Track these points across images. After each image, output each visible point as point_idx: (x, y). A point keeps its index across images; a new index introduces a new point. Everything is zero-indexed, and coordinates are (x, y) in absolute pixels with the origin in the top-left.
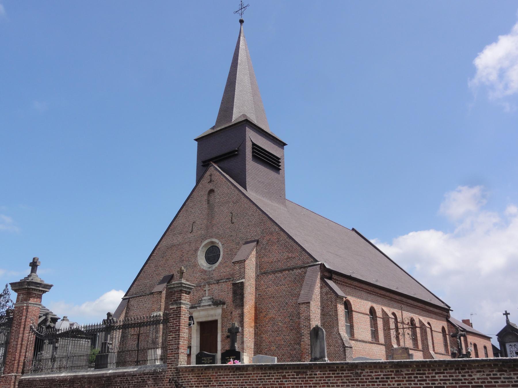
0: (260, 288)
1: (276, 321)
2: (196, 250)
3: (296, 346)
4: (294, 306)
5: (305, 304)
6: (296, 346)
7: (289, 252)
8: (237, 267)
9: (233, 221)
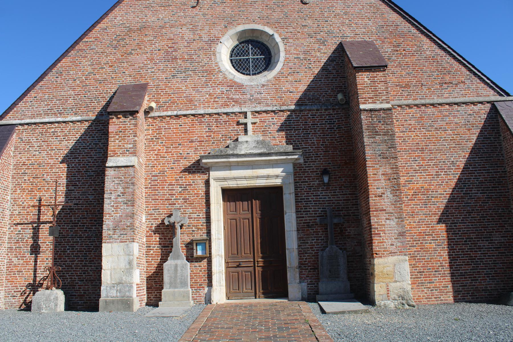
1: (432, 194)
2: (215, 41)
3: (481, 244)
4: (471, 169)
6: (481, 244)
8: (366, 80)
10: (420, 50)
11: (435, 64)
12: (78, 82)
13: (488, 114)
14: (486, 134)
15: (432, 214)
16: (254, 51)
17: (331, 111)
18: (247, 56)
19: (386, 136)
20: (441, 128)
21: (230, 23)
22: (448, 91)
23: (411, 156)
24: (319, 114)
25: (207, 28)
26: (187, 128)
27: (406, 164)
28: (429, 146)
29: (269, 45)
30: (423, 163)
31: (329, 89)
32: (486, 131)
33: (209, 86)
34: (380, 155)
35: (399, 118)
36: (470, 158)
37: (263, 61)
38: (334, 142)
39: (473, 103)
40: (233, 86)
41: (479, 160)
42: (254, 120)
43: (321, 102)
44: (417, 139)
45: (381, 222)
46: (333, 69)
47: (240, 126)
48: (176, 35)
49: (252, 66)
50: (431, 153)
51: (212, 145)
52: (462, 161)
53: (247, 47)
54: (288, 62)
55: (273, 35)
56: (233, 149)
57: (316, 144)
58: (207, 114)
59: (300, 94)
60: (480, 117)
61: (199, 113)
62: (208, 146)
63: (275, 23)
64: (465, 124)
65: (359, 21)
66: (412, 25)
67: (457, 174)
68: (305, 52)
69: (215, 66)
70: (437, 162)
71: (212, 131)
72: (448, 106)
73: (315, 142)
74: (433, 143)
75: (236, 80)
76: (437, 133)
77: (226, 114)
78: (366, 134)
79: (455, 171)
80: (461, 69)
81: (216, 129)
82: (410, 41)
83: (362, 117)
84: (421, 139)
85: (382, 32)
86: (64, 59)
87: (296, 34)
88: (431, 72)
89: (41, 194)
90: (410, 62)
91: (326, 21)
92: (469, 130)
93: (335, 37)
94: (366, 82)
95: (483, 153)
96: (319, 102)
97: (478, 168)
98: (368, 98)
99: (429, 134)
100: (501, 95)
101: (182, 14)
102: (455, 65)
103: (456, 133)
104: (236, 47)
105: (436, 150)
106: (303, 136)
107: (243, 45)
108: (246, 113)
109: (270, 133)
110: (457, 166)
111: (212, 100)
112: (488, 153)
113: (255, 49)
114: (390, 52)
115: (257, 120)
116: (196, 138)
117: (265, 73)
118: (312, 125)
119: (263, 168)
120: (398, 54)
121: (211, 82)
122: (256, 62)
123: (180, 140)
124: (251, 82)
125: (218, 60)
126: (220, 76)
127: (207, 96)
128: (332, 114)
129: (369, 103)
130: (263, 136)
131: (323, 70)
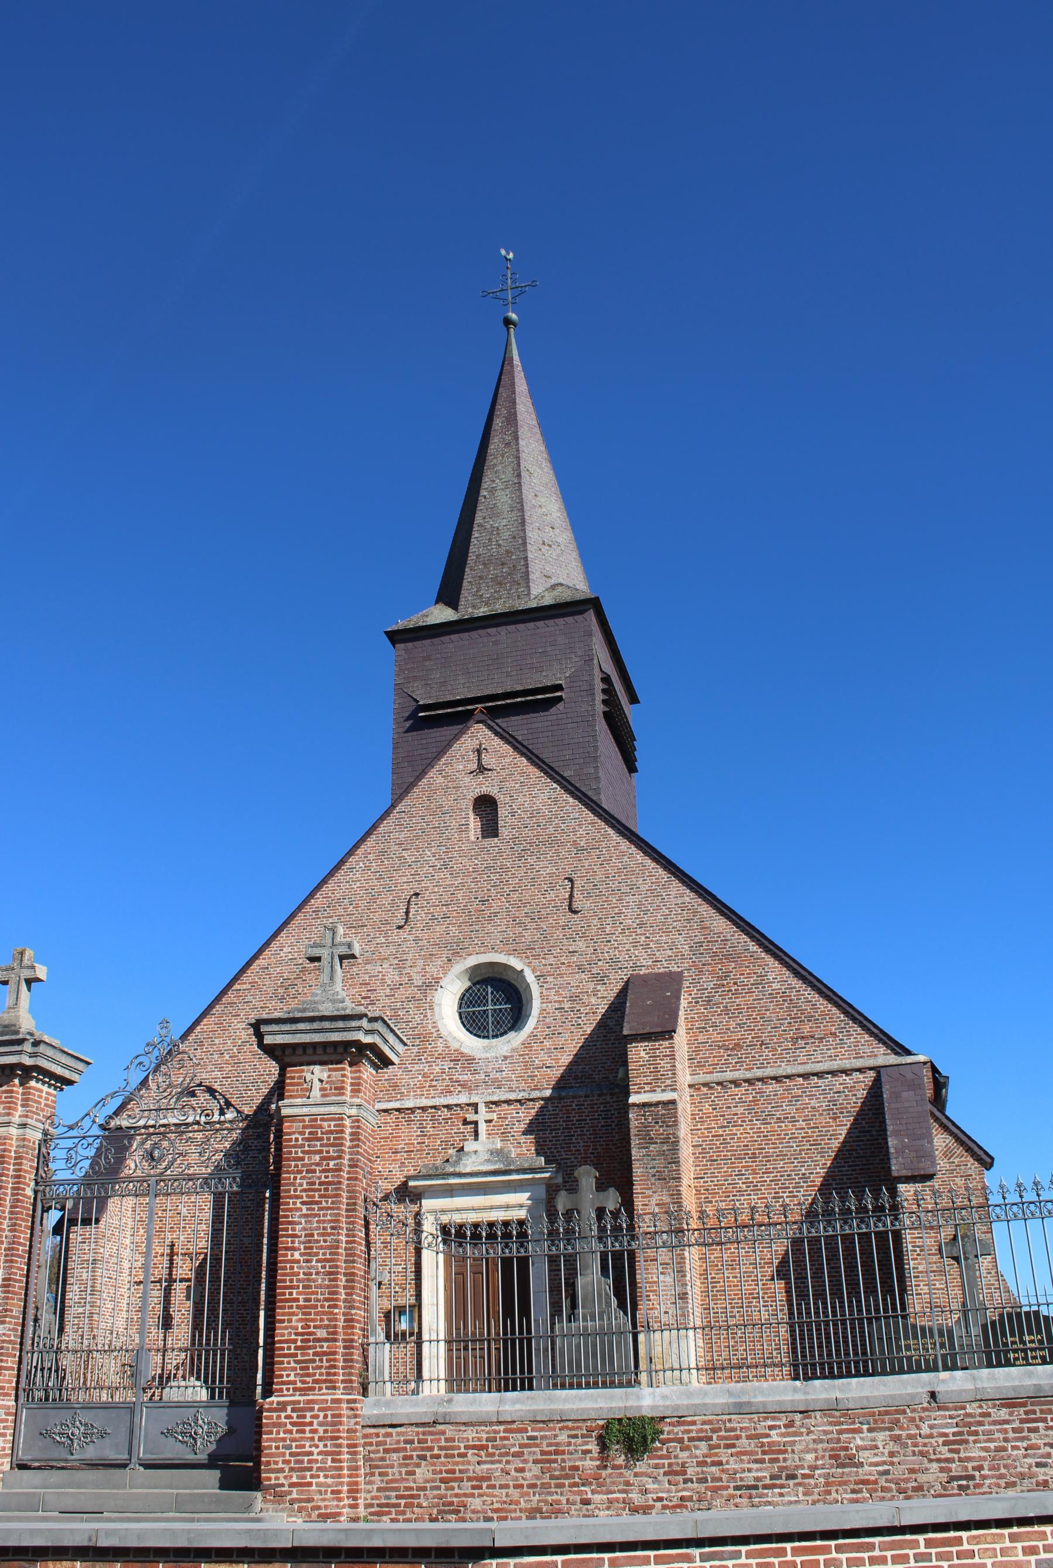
0: (699, 1127)
2: (432, 985)
5: (919, 1179)
7: (804, 1021)
8: (643, 1054)
9: (575, 906)
10: (761, 981)
11: (786, 1005)
12: (227, 1057)
13: (870, 1089)
14: (864, 1125)
15: (765, 1263)
16: (495, 996)
17: (608, 1098)
18: (484, 1005)
19: (665, 1145)
20: (788, 1118)
21: (456, 952)
22: (807, 1051)
23: (735, 1167)
24: (589, 1102)
25: (420, 963)
26: (388, 1130)
27: (725, 1180)
28: (765, 1149)
29: (519, 987)
30: (753, 1178)
31: (609, 1059)
32: (864, 1119)
33: (423, 1061)
34: (654, 1176)
35: (718, 1104)
36: (834, 1167)
37: (509, 1014)
38: (611, 1149)
39: (846, 1072)
40: (459, 1060)
41: (849, 1171)
42: (489, 1116)
43: (594, 1082)
44: (747, 1138)
45: (652, 1278)
46: (615, 1025)
47: (469, 1127)
48: (374, 976)
49: (493, 1023)
50: (769, 1161)
51: (426, 1158)
52: (820, 1173)
53: (484, 990)
54: (545, 1017)
55: (522, 970)
56: (454, 1166)
57: (582, 1151)
58: (419, 1108)
59: (561, 1070)
60: (855, 1095)
61: (406, 1106)
62: (420, 1158)
63: (527, 949)
64: (828, 1110)
65: (662, 936)
66: (750, 938)
67: (810, 1195)
68: (572, 997)
69: (433, 1027)
70: (777, 1176)
71: (426, 1135)
72: (801, 1079)
73: (582, 1148)
74: (773, 1144)
75: (463, 1050)
76: (779, 1127)
77: (448, 1107)
78: (634, 1142)
79: (807, 1191)
80: (831, 1010)
81: (432, 1131)
82: (746, 967)
83: (630, 1116)
84: (753, 1137)
85: (700, 954)
86: (205, 1020)
87: (559, 968)
88: (779, 1020)
89: (174, 1236)
90: (744, 1005)
91: (608, 941)
92: (834, 1119)
93: (621, 968)
94: (643, 1057)
95: (858, 1157)
96: (592, 1082)
97: (846, 1183)
98: (645, 1084)
99: (767, 1128)
100: (897, 1053)
101: (383, 940)
102: (821, 1004)
103: (812, 1125)
104: (467, 991)
105: (777, 1156)
106: (563, 1140)
107: (478, 987)
108: (477, 1104)
109: (513, 1136)
110: (811, 1182)
111: (428, 1084)
112: (865, 1157)
113: (497, 993)
114: (712, 988)
115: (494, 1116)
116: (403, 1146)
117: (512, 1035)
118: (577, 1120)
119: (501, 1194)
120: (724, 991)
121: (425, 1054)
122: (498, 1015)
123: (378, 1150)
124: (487, 1052)
125: (437, 1017)
126: (440, 1044)
127: (420, 1078)
128: (609, 1103)
129: (645, 1092)
130: (501, 1141)
131: (599, 1027)
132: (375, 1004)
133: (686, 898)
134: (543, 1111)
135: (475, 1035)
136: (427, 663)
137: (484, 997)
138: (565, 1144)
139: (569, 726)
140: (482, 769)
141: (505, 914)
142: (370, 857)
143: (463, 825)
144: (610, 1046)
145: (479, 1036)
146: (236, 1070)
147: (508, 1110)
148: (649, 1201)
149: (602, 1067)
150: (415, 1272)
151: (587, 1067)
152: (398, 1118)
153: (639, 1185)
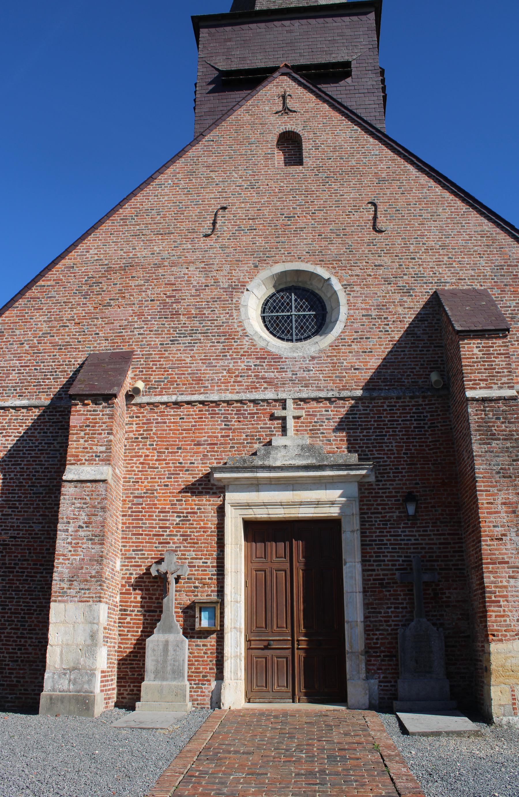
8: (476, 351)
9: (379, 226)
12: (27, 347)
16: (299, 304)
17: (420, 400)
18: (288, 311)
19: (508, 442)
25: (227, 267)
26: (191, 422)
29: (322, 296)
31: (417, 365)
33: (228, 357)
34: (498, 473)
37: (312, 320)
38: (424, 450)
40: (265, 358)
42: (298, 413)
43: (404, 385)
45: (501, 582)
46: (423, 334)
47: (276, 422)
49: (296, 328)
51: (230, 451)
53: (288, 297)
55: (329, 279)
57: (395, 451)
58: (224, 402)
59: (370, 373)
61: (211, 399)
62: (224, 451)
63: (333, 260)
65: (464, 258)
68: (379, 305)
69: (238, 326)
71: (230, 429)
73: (394, 448)
77: (255, 402)
78: (475, 437)
81: (237, 425)
83: (470, 410)
85: (501, 275)
86: (7, 312)
87: (365, 279)
91: (412, 259)
93: (426, 283)
96: (401, 385)
98: (480, 380)
101: (190, 246)
104: (271, 297)
106: (375, 439)
108: (285, 400)
109: (323, 433)
111: (233, 380)
113: (301, 300)
115: (303, 413)
116: (206, 438)
117: (317, 338)
118: (389, 421)
119: (311, 490)
121: (231, 351)
122: (302, 321)
124: (294, 352)
125: (243, 317)
126: (246, 341)
127: (225, 374)
128: (421, 405)
129: (480, 388)
130: (311, 437)
131: (407, 334)
132: (180, 302)
133: (485, 227)
134: (354, 410)
135: (279, 338)
136: (228, 43)
137: (288, 304)
138: (377, 443)
139: (357, 95)
140: (287, 111)
141: (310, 229)
142: (179, 176)
143: (269, 154)
144: (418, 352)
145: (282, 339)
146: (34, 360)
147: (316, 408)
148: (494, 500)
149: (411, 372)
150: (218, 567)
151: (396, 371)
152: (202, 411)
153: (483, 482)
